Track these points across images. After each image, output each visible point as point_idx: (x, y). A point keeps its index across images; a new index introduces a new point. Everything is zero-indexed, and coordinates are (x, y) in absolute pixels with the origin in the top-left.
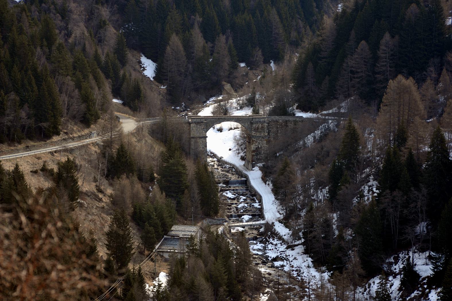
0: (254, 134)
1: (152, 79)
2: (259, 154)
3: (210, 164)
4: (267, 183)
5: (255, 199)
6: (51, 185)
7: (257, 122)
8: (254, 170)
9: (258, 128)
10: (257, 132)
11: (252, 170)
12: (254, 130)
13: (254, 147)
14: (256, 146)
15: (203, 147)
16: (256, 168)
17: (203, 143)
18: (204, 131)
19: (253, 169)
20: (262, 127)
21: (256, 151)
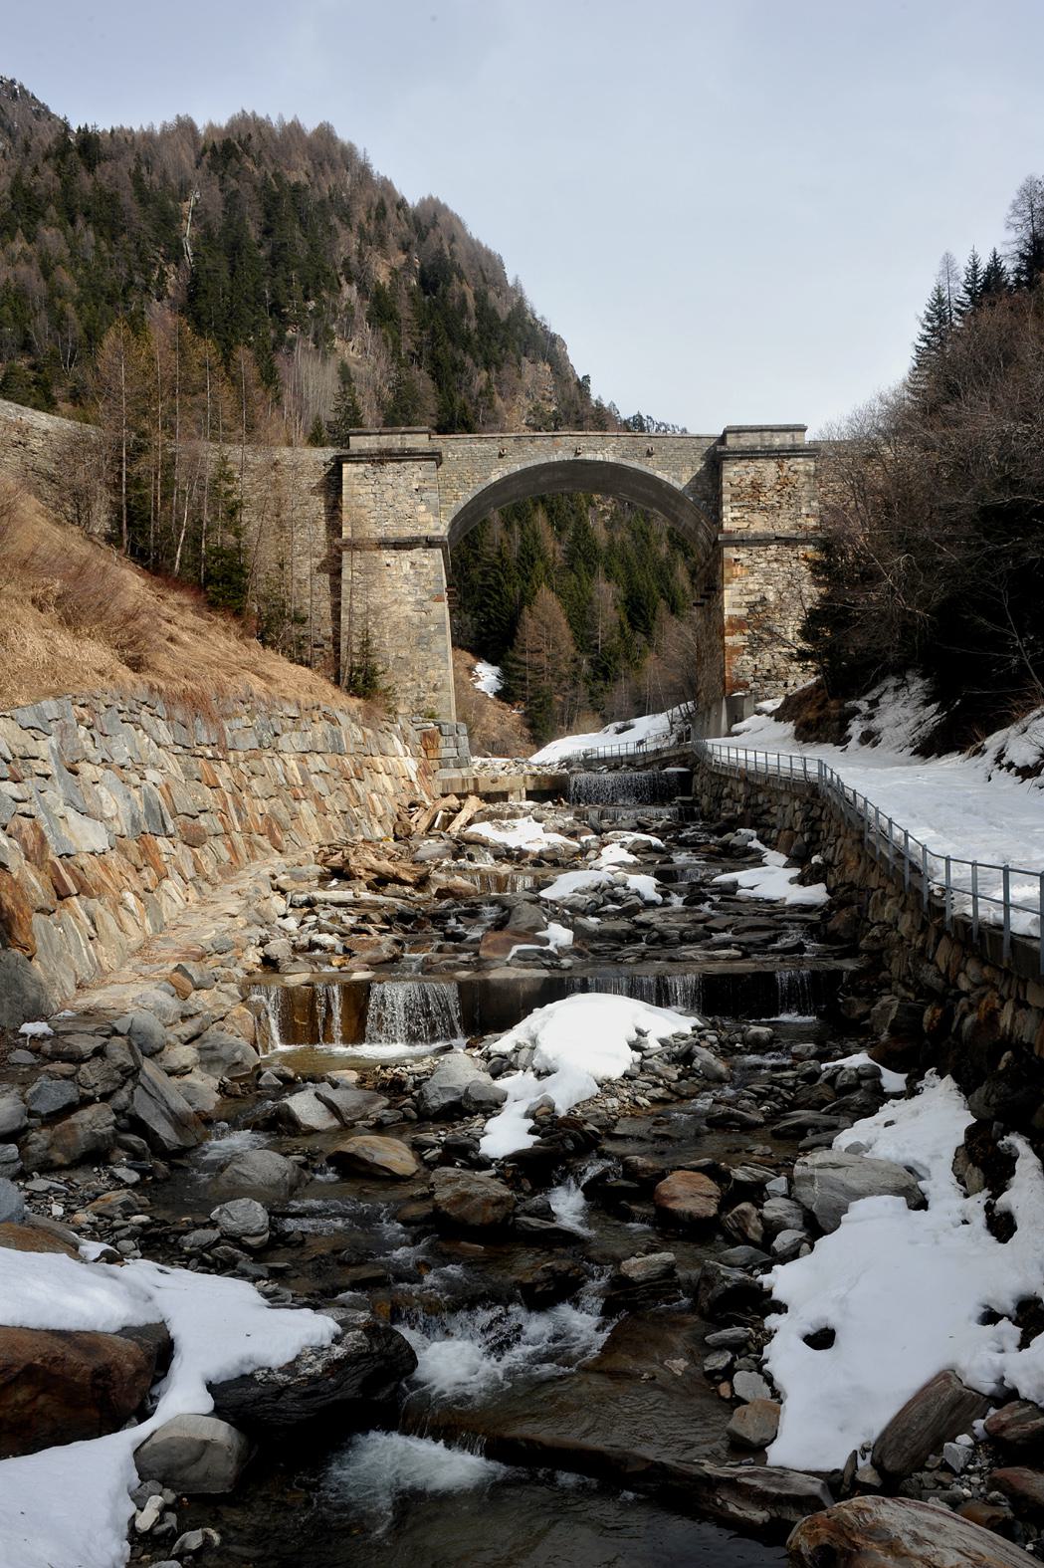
0: (734, 519)
1: (491, 695)
2: (767, 644)
3: (565, 886)
4: (516, 705)
5: (756, 844)
6: (818, 584)
7: (750, 454)
8: (737, 734)
9: (756, 486)
10: (753, 510)
11: (730, 734)
12: (736, 497)
13: (738, 599)
14: (751, 592)
15: (420, 603)
16: (792, 723)
17: (418, 574)
18: (427, 502)
19: (736, 727)
20: (784, 482)
21: (749, 626)
